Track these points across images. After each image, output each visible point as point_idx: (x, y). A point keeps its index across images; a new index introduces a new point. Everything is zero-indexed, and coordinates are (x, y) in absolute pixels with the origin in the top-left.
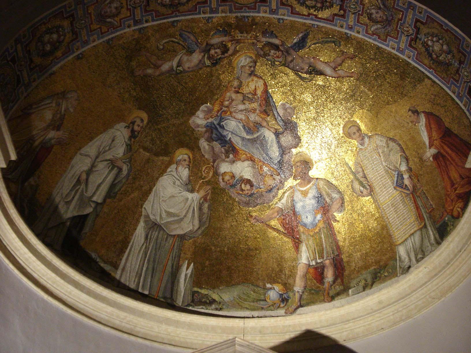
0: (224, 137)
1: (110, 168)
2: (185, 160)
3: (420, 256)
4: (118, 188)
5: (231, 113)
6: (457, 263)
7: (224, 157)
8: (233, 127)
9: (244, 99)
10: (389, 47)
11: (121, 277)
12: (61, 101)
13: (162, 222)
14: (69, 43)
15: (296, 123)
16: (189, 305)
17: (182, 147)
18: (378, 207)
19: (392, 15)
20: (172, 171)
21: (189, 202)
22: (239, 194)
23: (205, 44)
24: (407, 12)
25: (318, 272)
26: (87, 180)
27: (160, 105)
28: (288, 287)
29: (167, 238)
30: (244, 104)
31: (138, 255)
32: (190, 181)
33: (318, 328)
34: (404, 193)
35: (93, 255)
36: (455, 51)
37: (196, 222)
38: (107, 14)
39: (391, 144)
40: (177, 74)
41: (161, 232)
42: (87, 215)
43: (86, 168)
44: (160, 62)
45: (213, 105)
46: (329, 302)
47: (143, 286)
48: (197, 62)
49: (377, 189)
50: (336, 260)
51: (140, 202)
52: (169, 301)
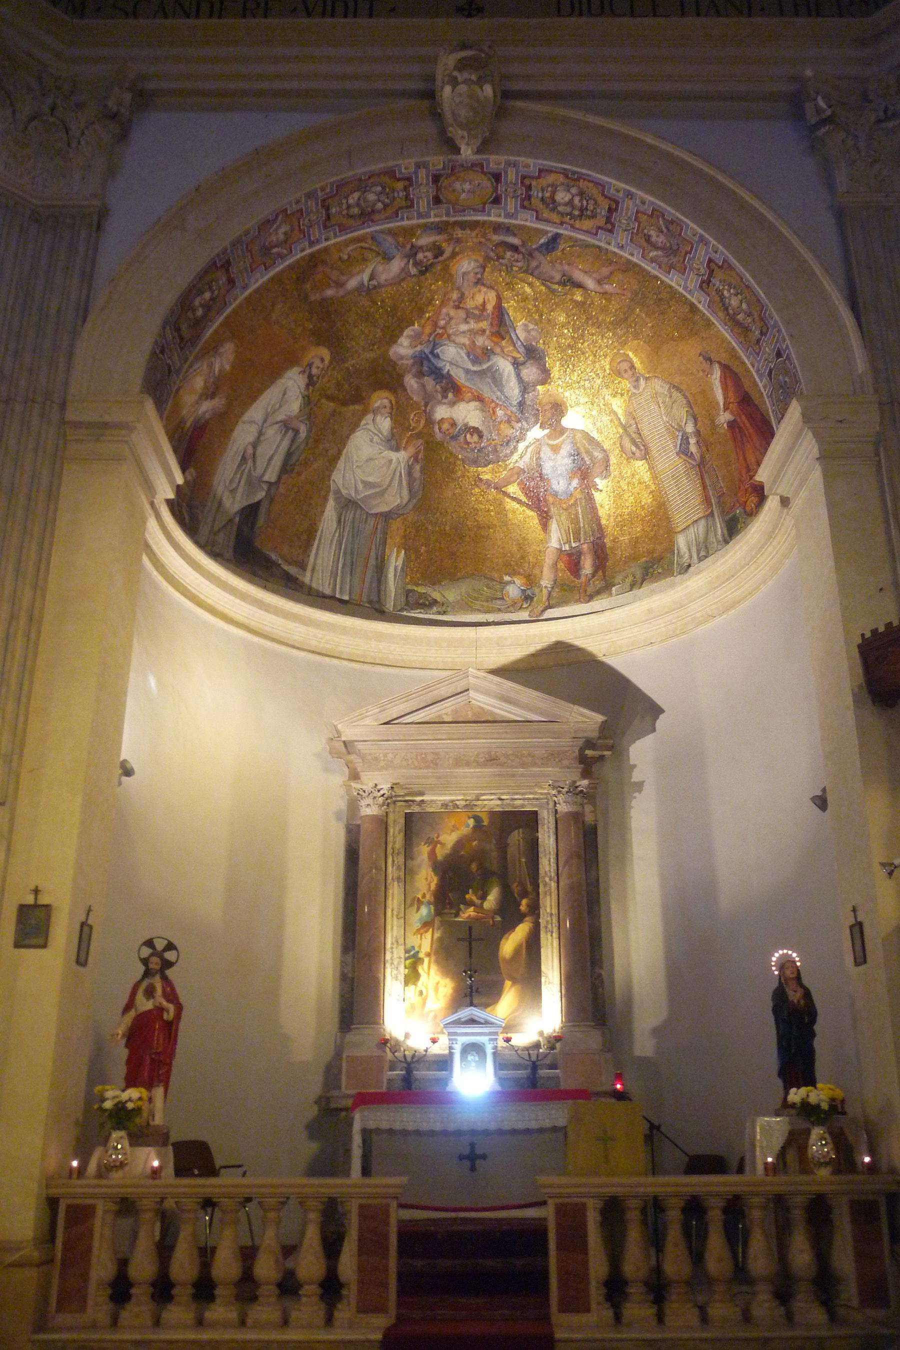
0: (440, 369)
2: (385, 407)
3: (703, 553)
4: (294, 458)
5: (449, 336)
7: (440, 396)
8: (452, 356)
9: (467, 317)
10: (673, 280)
11: (311, 580)
12: (213, 360)
15: (543, 351)
16: (402, 610)
17: (381, 389)
18: (655, 477)
21: (393, 466)
23: (409, 247)
25: (573, 561)
26: (254, 454)
28: (531, 580)
29: (367, 518)
30: (468, 323)
32: (393, 435)
35: (274, 557)
36: (756, 316)
37: (405, 493)
39: (676, 394)
40: (369, 290)
41: (358, 512)
42: (259, 503)
44: (344, 278)
47: (341, 592)
49: (654, 452)
50: (597, 544)
51: (327, 473)
52: (377, 606)
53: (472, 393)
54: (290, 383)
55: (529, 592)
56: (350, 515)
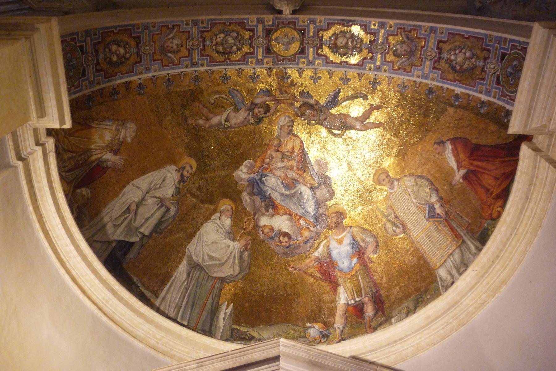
0: (264, 192)
1: (159, 206)
2: (228, 211)
6: (507, 254)
7: (264, 210)
8: (273, 184)
11: (160, 305)
12: (120, 128)
13: (204, 264)
14: (133, 64)
19: (415, 46)
20: (215, 219)
22: (278, 245)
24: (429, 37)
26: (136, 211)
27: (208, 155)
28: (328, 325)
30: (283, 161)
31: (179, 289)
32: (232, 230)
33: (363, 354)
34: (437, 221)
35: (135, 279)
38: (169, 48)
39: (420, 181)
41: (203, 273)
42: (132, 244)
43: (137, 200)
44: (211, 115)
45: (256, 161)
46: (372, 333)
47: (182, 317)
48: (243, 119)
49: (409, 226)
51: (184, 243)
53: (285, 210)
54: (169, 175)
55: (325, 332)
56: (196, 274)
